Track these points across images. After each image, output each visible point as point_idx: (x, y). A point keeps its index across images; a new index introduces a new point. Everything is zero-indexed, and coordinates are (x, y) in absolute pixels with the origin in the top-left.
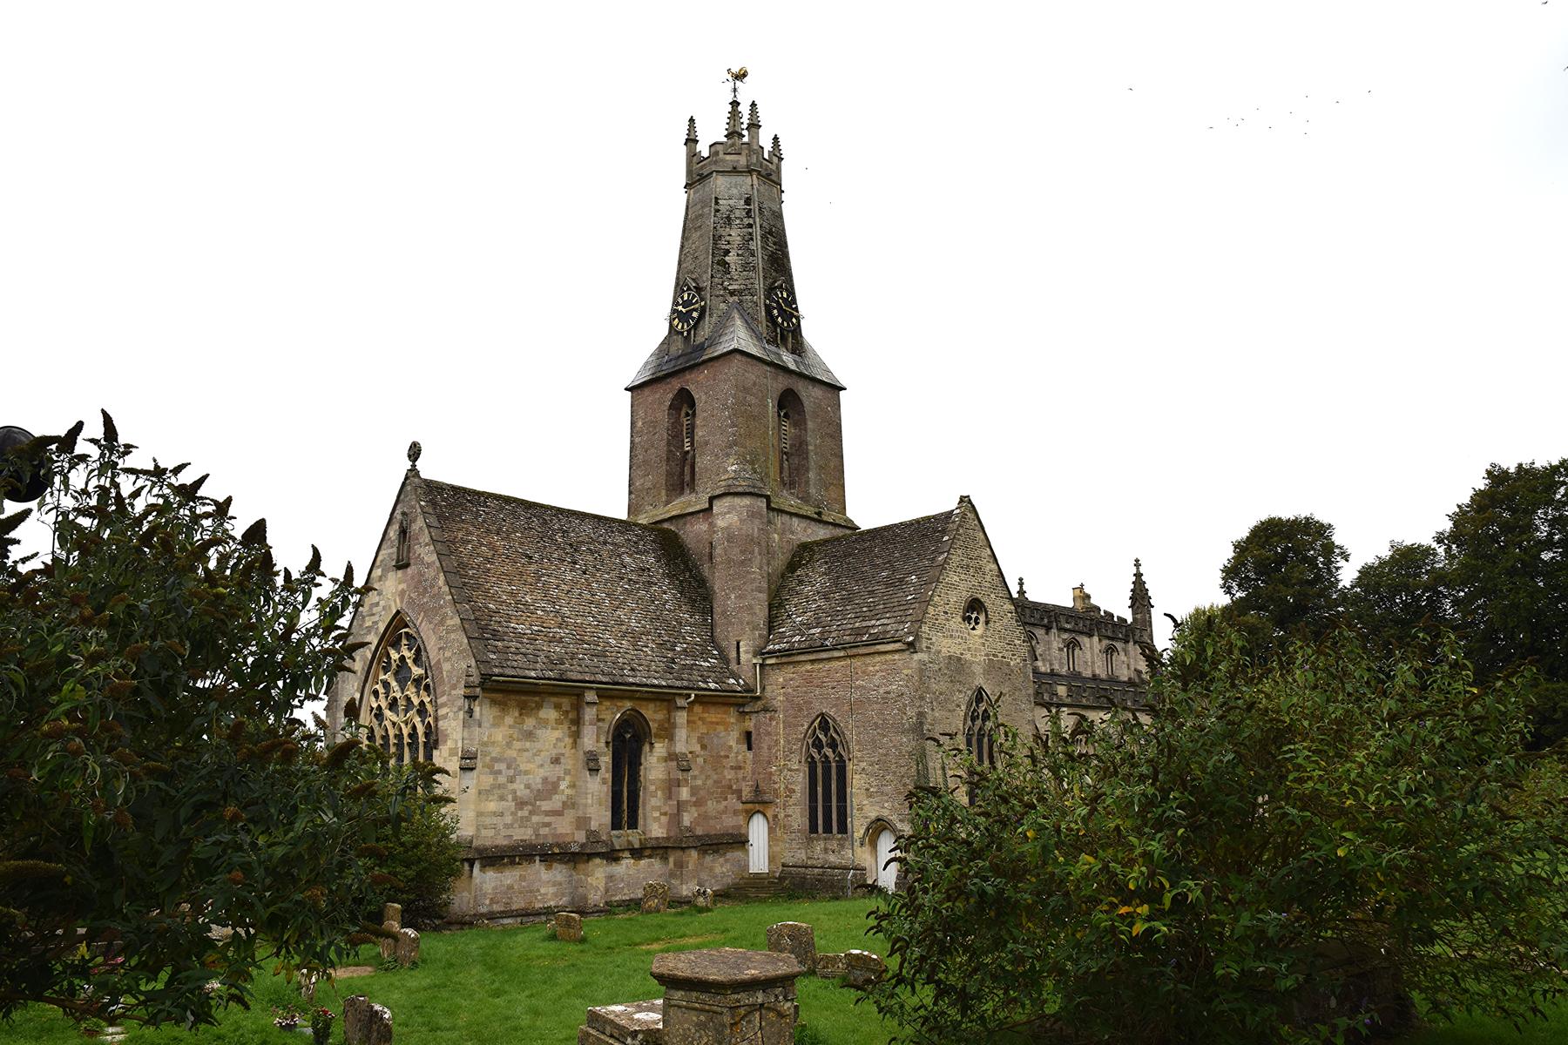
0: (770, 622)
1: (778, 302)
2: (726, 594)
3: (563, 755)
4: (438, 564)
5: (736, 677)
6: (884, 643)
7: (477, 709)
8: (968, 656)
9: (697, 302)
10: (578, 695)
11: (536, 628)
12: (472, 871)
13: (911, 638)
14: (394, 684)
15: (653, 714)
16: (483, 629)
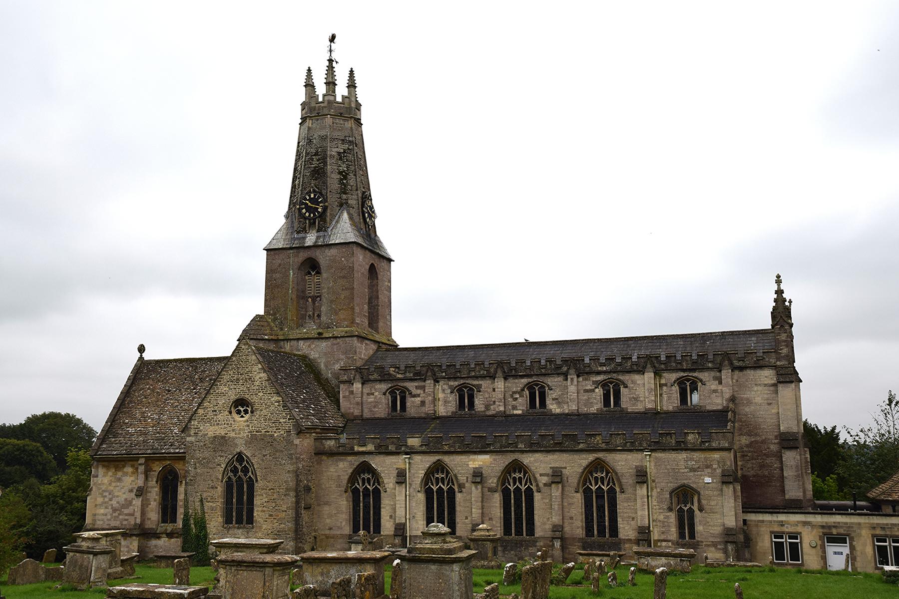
8: (232, 435)
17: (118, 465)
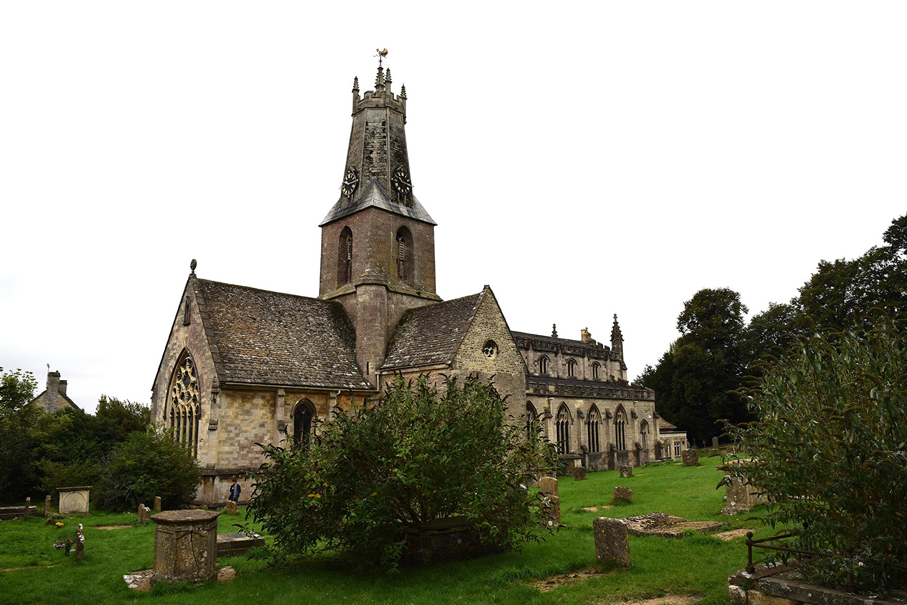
0: (387, 352)
1: (398, 179)
2: (362, 338)
3: (266, 422)
4: (202, 324)
5: (366, 381)
6: (437, 364)
7: (218, 399)
9: (354, 179)
10: (275, 392)
11: (254, 357)
12: (214, 482)
13: (450, 362)
14: (183, 385)
15: (317, 401)
16: (225, 357)
17: (246, 395)
